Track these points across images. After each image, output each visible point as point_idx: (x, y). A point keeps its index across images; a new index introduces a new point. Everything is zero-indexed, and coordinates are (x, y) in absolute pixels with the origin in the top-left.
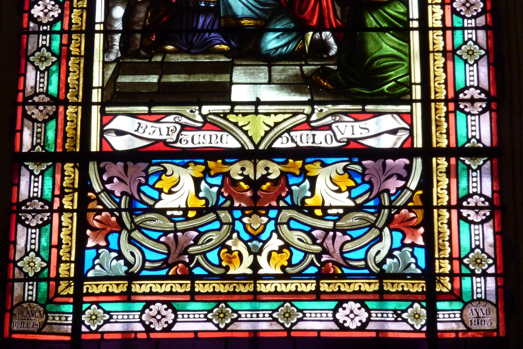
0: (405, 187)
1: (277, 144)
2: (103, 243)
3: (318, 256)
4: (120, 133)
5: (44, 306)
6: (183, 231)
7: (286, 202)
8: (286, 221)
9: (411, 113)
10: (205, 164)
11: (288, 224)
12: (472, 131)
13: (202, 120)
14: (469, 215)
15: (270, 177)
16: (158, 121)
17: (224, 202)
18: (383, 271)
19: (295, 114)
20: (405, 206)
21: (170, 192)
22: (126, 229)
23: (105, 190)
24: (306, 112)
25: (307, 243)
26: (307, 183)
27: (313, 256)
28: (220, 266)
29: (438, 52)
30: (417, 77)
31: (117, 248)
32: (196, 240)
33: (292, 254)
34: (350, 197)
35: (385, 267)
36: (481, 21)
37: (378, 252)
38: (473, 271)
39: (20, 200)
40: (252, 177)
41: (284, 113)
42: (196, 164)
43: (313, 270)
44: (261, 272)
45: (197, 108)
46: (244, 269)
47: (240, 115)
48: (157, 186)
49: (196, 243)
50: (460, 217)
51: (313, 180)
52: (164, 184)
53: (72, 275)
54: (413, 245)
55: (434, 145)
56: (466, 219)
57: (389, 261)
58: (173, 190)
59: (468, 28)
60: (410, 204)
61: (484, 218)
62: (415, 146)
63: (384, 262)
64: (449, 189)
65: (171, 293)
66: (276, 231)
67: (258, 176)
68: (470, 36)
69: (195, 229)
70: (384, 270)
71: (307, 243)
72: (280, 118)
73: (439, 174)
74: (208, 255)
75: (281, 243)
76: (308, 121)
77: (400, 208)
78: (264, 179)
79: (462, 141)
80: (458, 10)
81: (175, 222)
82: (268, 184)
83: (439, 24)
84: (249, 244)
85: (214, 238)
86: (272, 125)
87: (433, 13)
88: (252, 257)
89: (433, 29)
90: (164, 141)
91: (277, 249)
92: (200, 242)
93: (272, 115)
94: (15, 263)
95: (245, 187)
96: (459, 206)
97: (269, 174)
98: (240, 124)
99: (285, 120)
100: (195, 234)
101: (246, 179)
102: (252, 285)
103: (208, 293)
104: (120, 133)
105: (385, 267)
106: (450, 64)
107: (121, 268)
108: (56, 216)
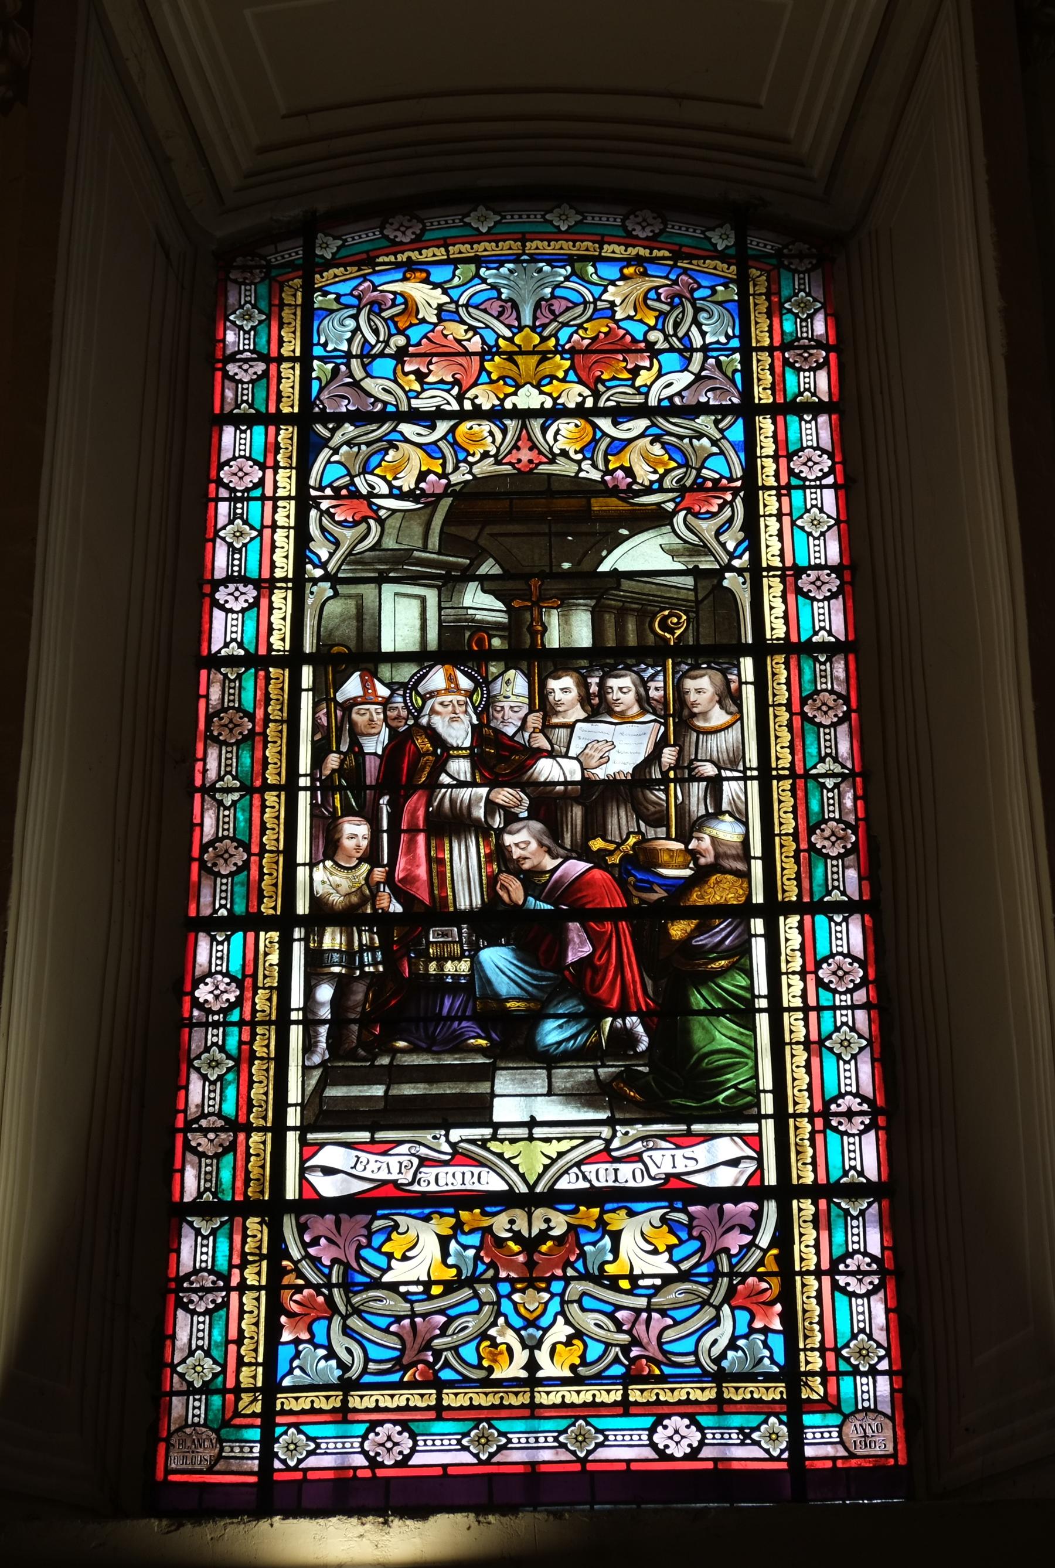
0: (752, 1244)
2: (305, 1336)
4: (328, 1171)
6: (425, 1316)
7: (576, 1270)
8: (577, 1298)
9: (759, 1134)
10: (456, 1215)
11: (579, 1302)
13: (449, 1150)
15: (552, 1233)
16: (385, 1153)
17: (485, 1271)
18: (721, 1369)
19: (587, 1139)
20: (753, 1272)
21: (405, 1258)
22: (340, 1314)
23: (307, 1256)
24: (603, 1136)
25: (609, 1331)
26: (607, 1241)
27: (618, 1349)
28: (480, 1366)
31: (326, 1343)
32: (444, 1328)
34: (670, 1261)
35: (725, 1364)
38: (190, 1384)
40: (526, 1234)
41: (571, 1138)
42: (442, 1215)
43: (617, 1370)
45: (443, 1132)
46: (515, 1370)
47: (507, 1142)
50: (835, 1286)
52: (396, 1245)
54: (766, 1331)
56: (843, 1290)
57: (731, 1354)
58: (409, 1254)
59: (841, 1008)
60: (761, 1269)
62: (766, 1183)
63: (723, 1355)
65: (407, 1408)
66: (562, 1313)
67: (535, 1232)
68: (844, 1019)
69: (442, 1312)
70: (724, 1368)
71: (609, 1331)
72: (565, 1145)
74: (462, 1350)
75: (571, 1331)
76: (607, 1150)
77: (745, 1276)
78: (544, 1236)
82: (550, 1243)
84: (523, 1333)
85: (470, 1325)
86: (554, 1156)
88: (527, 1352)
89: (790, 1009)
91: (564, 1340)
92: (450, 1331)
93: (554, 1141)
94: (173, 1367)
95: (516, 1248)
96: (833, 1271)
97: (550, 1229)
99: (573, 1148)
100: (442, 1319)
101: (517, 1237)
102: (528, 1395)
103: (462, 1408)
104: (328, 1171)
105: (725, 1364)
107: (331, 1371)
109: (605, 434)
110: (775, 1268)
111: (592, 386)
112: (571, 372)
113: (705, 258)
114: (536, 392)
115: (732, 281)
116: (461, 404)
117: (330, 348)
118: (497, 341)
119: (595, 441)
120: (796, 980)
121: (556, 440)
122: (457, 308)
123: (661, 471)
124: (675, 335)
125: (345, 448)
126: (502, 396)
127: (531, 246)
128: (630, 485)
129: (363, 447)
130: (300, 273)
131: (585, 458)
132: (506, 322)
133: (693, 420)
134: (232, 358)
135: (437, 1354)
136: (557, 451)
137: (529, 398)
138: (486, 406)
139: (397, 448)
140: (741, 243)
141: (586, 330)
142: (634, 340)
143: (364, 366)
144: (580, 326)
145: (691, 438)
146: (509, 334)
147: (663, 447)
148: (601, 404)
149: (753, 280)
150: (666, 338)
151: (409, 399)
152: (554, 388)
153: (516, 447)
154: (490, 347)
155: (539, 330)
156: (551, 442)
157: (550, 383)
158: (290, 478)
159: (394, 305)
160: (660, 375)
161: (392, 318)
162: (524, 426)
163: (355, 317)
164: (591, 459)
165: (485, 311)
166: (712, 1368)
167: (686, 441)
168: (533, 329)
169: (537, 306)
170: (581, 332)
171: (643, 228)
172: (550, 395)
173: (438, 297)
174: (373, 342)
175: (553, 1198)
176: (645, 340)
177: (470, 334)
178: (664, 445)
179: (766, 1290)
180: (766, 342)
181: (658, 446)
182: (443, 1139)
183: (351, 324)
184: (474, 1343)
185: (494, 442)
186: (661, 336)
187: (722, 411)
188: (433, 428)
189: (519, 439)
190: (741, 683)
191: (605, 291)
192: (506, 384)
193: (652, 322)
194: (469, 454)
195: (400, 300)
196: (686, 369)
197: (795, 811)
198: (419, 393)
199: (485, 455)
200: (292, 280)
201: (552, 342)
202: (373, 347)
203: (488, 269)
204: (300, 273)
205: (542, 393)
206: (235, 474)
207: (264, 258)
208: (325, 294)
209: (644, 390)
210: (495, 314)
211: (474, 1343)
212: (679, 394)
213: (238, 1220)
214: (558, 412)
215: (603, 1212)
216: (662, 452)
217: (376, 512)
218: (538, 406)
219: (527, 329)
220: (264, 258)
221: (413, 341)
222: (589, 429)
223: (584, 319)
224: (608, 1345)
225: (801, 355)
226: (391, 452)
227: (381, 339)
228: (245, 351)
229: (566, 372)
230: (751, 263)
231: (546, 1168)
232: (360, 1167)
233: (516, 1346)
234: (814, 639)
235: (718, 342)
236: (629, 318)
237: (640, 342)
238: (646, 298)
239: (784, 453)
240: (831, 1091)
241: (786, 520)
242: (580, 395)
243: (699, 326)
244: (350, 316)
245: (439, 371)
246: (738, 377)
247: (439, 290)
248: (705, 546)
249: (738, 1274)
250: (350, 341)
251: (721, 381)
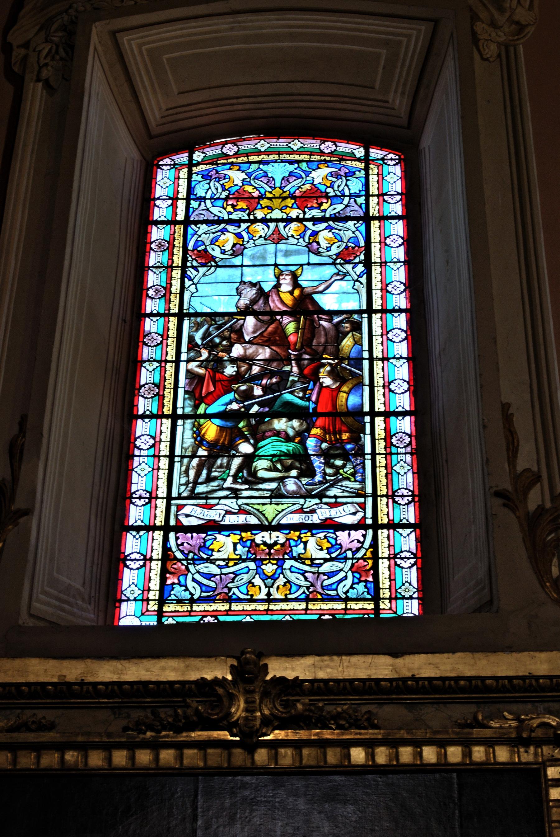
0: (362, 547)
1: (283, 522)
3: (308, 588)
4: (187, 516)
6: (225, 574)
7: (289, 556)
8: (289, 568)
9: (365, 503)
10: (240, 535)
11: (290, 569)
16: (210, 509)
18: (347, 597)
19: (294, 504)
20: (362, 558)
21: (219, 551)
26: (302, 545)
27: (305, 588)
28: (247, 594)
32: (233, 579)
35: (348, 594)
36: (409, 449)
38: (128, 598)
41: (288, 504)
42: (235, 534)
43: (303, 596)
44: (271, 597)
46: (263, 596)
48: (210, 548)
51: (305, 543)
52: (215, 546)
54: (366, 581)
56: (399, 566)
57: (351, 590)
58: (220, 550)
59: (400, 454)
63: (348, 591)
64: (383, 369)
67: (272, 542)
68: (402, 458)
69: (233, 573)
75: (286, 580)
77: (359, 559)
78: (276, 543)
81: (221, 569)
83: (378, 260)
86: (280, 510)
88: (267, 589)
89: (380, 454)
90: (214, 521)
91: (283, 584)
92: (236, 581)
94: (122, 592)
97: (278, 540)
98: (260, 510)
99: (288, 507)
101: (265, 543)
104: (187, 516)
105: (348, 594)
107: (187, 595)
113: (352, 160)
114: (280, 212)
118: (265, 192)
119: (305, 231)
120: (379, 338)
123: (332, 243)
131: (301, 238)
135: (230, 589)
136: (289, 235)
137: (277, 214)
140: (367, 153)
141: (302, 188)
142: (322, 192)
144: (300, 187)
146: (270, 190)
150: (334, 191)
153: (273, 234)
154: (262, 195)
157: (286, 209)
158: (172, 367)
159: (225, 179)
160: (331, 205)
161: (223, 184)
163: (209, 184)
166: (343, 596)
167: (342, 231)
168: (280, 188)
172: (285, 213)
174: (215, 193)
175: (279, 527)
176: (325, 192)
179: (366, 565)
186: (332, 190)
187: (357, 219)
188: (239, 227)
190: (367, 550)
193: (329, 185)
195: (227, 177)
197: (387, 485)
199: (260, 237)
202: (215, 195)
205: (282, 212)
206: (150, 340)
212: (339, 213)
214: (288, 220)
215: (301, 534)
221: (232, 193)
222: (302, 226)
223: (302, 183)
224: (300, 586)
229: (293, 204)
230: (371, 162)
231: (277, 515)
233: (263, 587)
234: (396, 410)
236: (320, 183)
237: (323, 192)
238: (327, 176)
239: (385, 332)
240: (395, 488)
241: (380, 176)
245: (242, 205)
246: (363, 206)
247: (244, 174)
251: (357, 208)
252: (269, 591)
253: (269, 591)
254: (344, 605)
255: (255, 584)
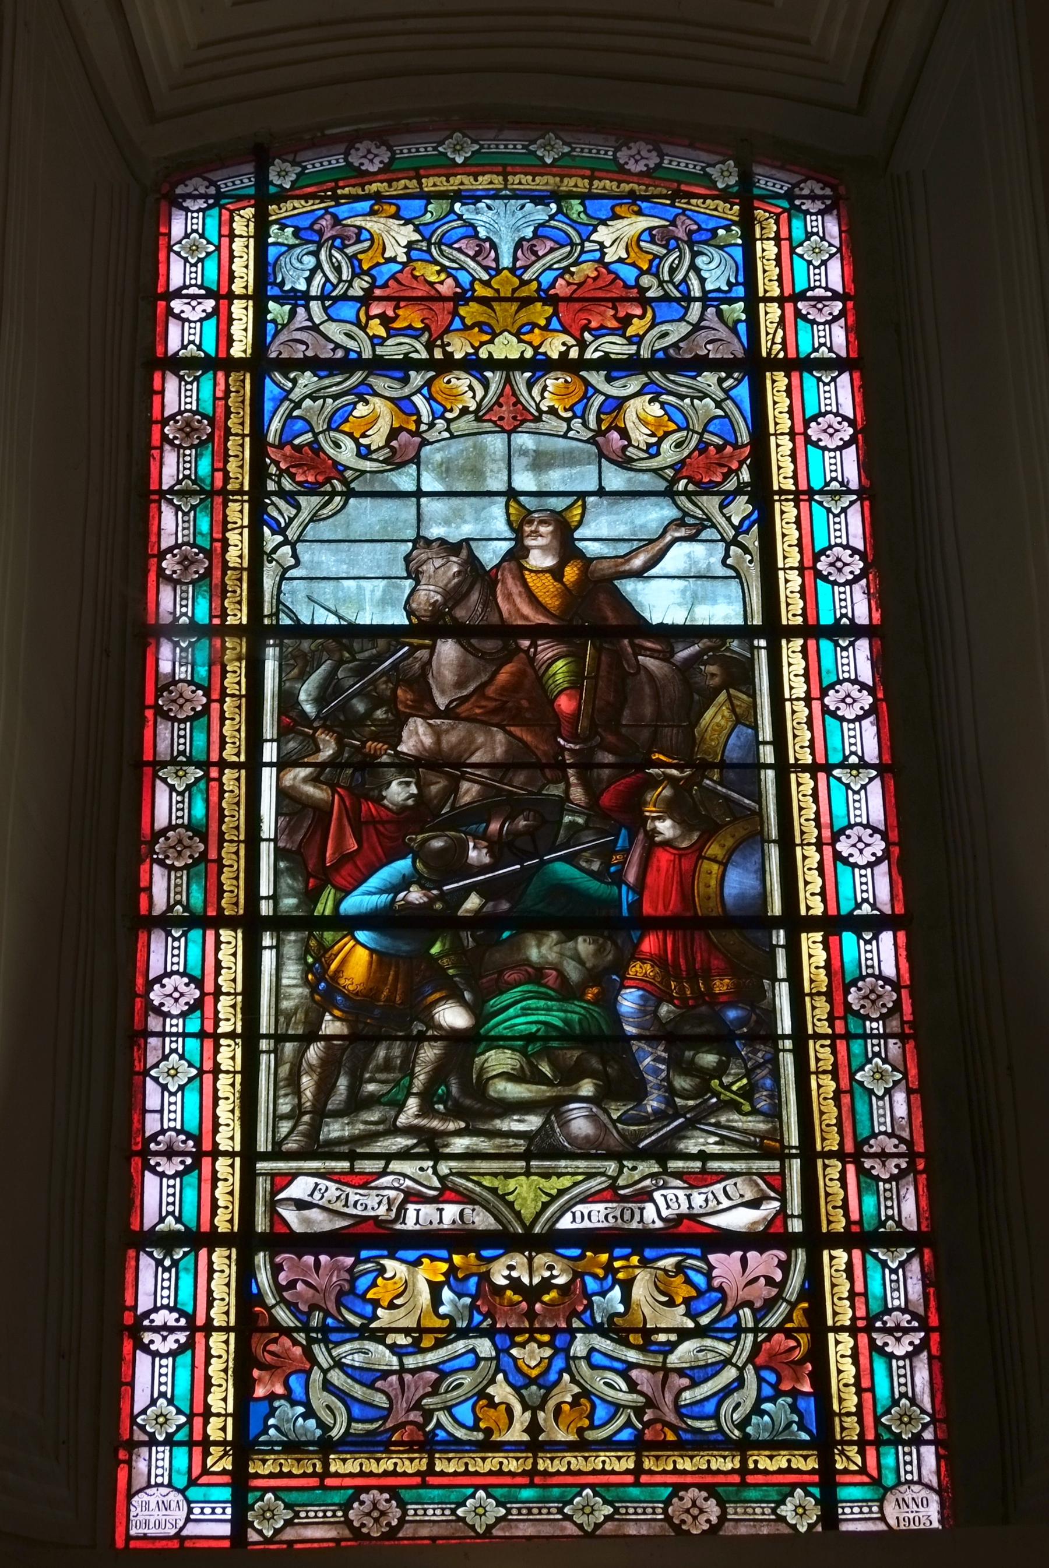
1: (565, 1223)
2: (279, 1390)
5: (182, 1492)
6: (414, 1372)
10: (449, 1260)
12: (851, 744)
13: (437, 1184)
14: (873, 1168)
15: (554, 1281)
17: (481, 1322)
18: (747, 1436)
19: (589, 1176)
20: (780, 1328)
21: (392, 1306)
22: (320, 1367)
23: (283, 1300)
28: (475, 1428)
29: (798, 699)
30: (767, 733)
31: (304, 1398)
32: (436, 1385)
33: (594, 1407)
34: (688, 1314)
35: (749, 1430)
37: (738, 1405)
39: (172, 289)
40: (526, 1280)
41: (573, 1174)
42: (433, 1259)
43: (626, 1435)
45: (431, 1163)
46: (517, 1433)
49: (434, 1393)
52: (382, 1292)
53: (230, 1437)
54: (795, 1393)
55: (803, 912)
56: (804, 318)
57: (755, 1419)
58: (397, 1302)
59: (872, 1036)
61: (910, 1348)
63: (746, 1421)
65: (394, 1473)
67: (536, 1280)
69: (433, 1368)
70: (749, 1435)
72: (566, 1182)
73: (818, 1023)
75: (577, 1390)
76: (613, 1187)
77: (771, 1332)
78: (546, 1285)
79: (846, 907)
80: (845, 854)
82: (554, 1294)
85: (466, 1382)
86: (554, 1192)
87: (787, 581)
93: (554, 1178)
96: (869, 1329)
97: (553, 1277)
100: (433, 1376)
101: (515, 1284)
103: (455, 1474)
104: (301, 1205)
105: (749, 1430)
106: (796, 381)
108: (199, 1337)
109: (597, 391)
110: (805, 1324)
111: (577, 334)
112: (554, 320)
113: (705, 198)
115: (735, 223)
116: (430, 352)
117: (287, 287)
118: (472, 283)
119: (586, 397)
121: (543, 398)
122: (429, 247)
123: (660, 433)
124: (671, 281)
125: (308, 402)
126: (477, 344)
127: (514, 180)
128: (624, 448)
129: (329, 401)
130: (252, 202)
131: (575, 416)
132: (484, 263)
133: (694, 378)
134: (178, 294)
137: (506, 348)
138: (458, 356)
139: (367, 402)
140: (746, 180)
141: (572, 274)
142: (626, 286)
143: (325, 309)
145: (692, 398)
147: (662, 408)
148: (588, 355)
149: (760, 222)
150: (661, 283)
151: (373, 346)
152: (536, 337)
153: (498, 403)
154: (465, 291)
155: (519, 272)
156: (538, 399)
157: (531, 331)
159: (358, 241)
161: (355, 256)
162: (508, 381)
163: (316, 254)
164: (583, 417)
165: (460, 250)
167: (688, 401)
169: (519, 245)
170: (567, 276)
171: (637, 162)
172: (530, 344)
173: (408, 234)
174: (335, 281)
177: (443, 276)
178: (663, 405)
179: (793, 1348)
180: (776, 292)
181: (657, 405)
182: (430, 1171)
183: (310, 261)
184: (470, 1403)
185: (474, 397)
188: (405, 381)
189: (501, 395)
191: (595, 230)
192: (481, 331)
194: (446, 410)
195: (365, 235)
196: (682, 319)
198: (385, 340)
200: (244, 208)
201: (534, 285)
202: (335, 287)
203: (463, 204)
204: (252, 202)
205: (520, 341)
207: (213, 183)
208: (283, 227)
209: (635, 339)
210: (472, 253)
211: (470, 1403)
212: (675, 345)
213: (203, 1253)
216: (662, 412)
217: (341, 473)
218: (517, 356)
219: (506, 272)
220: (213, 183)
221: (379, 282)
225: (814, 306)
226: (360, 406)
227: (344, 277)
228: (191, 285)
229: (549, 320)
230: (756, 204)
231: (545, 1206)
232: (317, 1195)
233: (517, 1408)
235: (719, 290)
236: (621, 260)
238: (639, 240)
242: (564, 344)
243: (698, 271)
244: (308, 253)
245: (410, 316)
246: (742, 328)
247: (411, 227)
248: (709, 519)
249: (763, 1330)
250: (309, 280)
251: (723, 333)
252: (534, 1419)
253: (534, 1419)
254: (632, 1460)
255: (497, 1400)
